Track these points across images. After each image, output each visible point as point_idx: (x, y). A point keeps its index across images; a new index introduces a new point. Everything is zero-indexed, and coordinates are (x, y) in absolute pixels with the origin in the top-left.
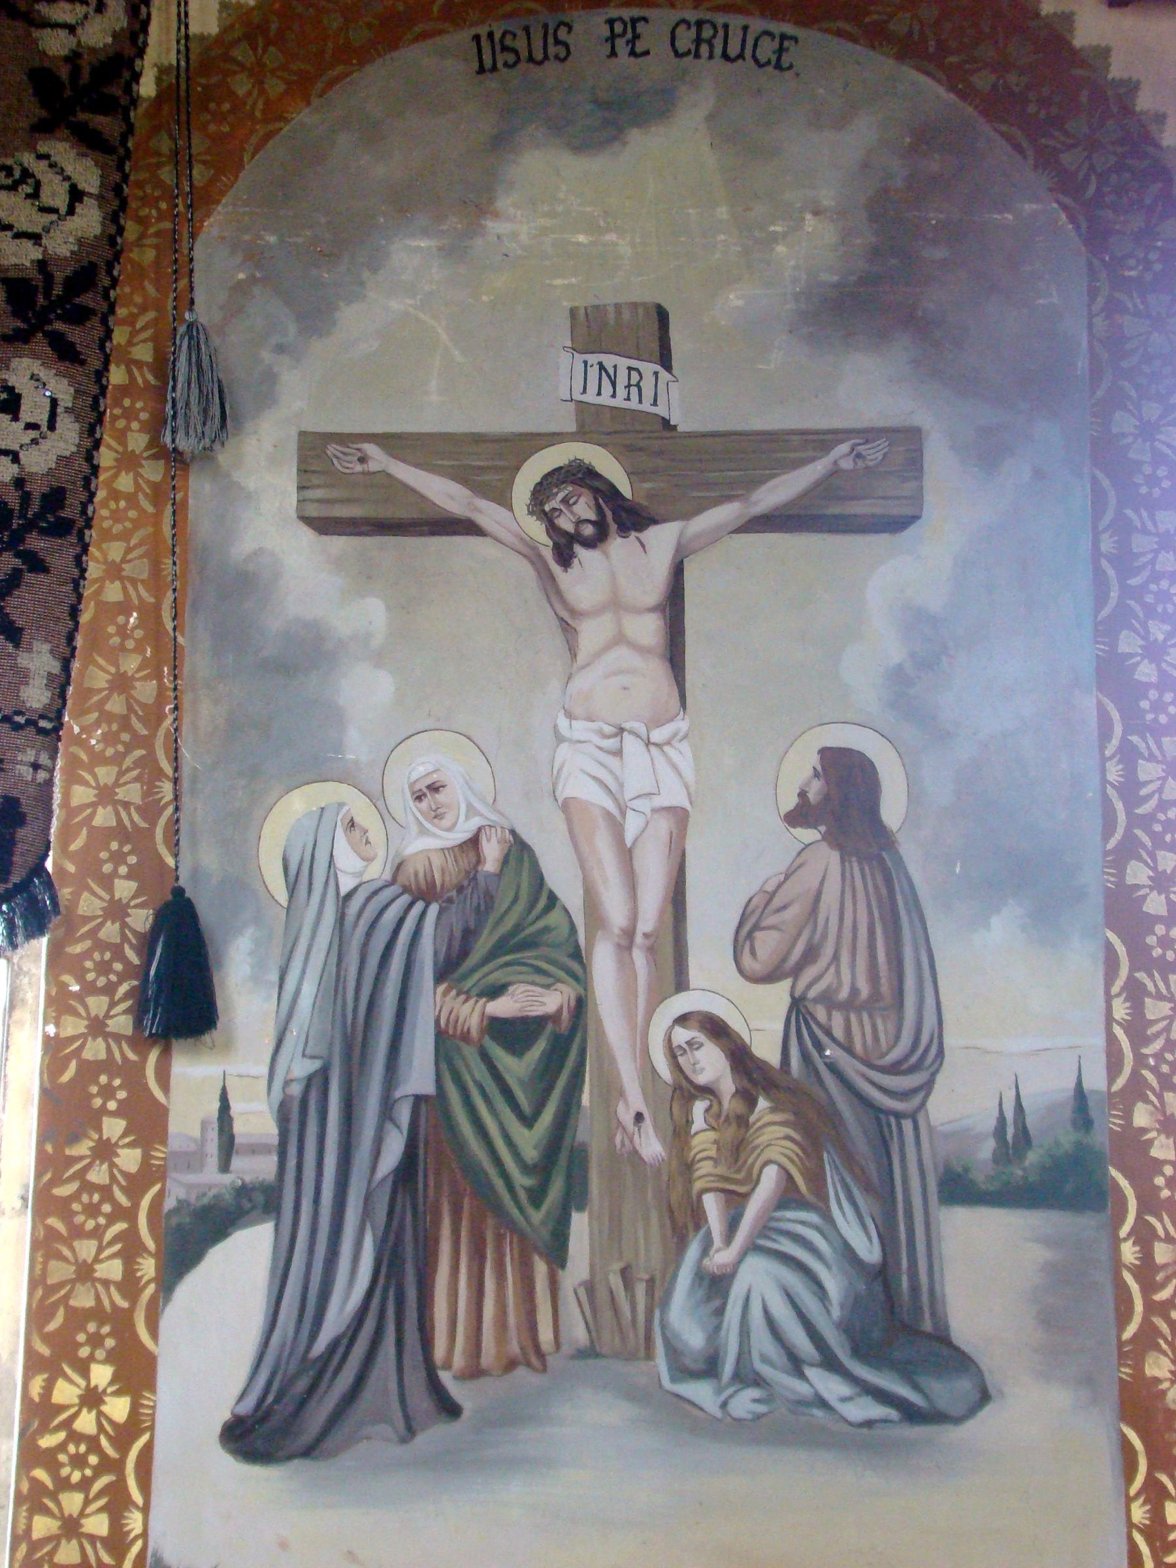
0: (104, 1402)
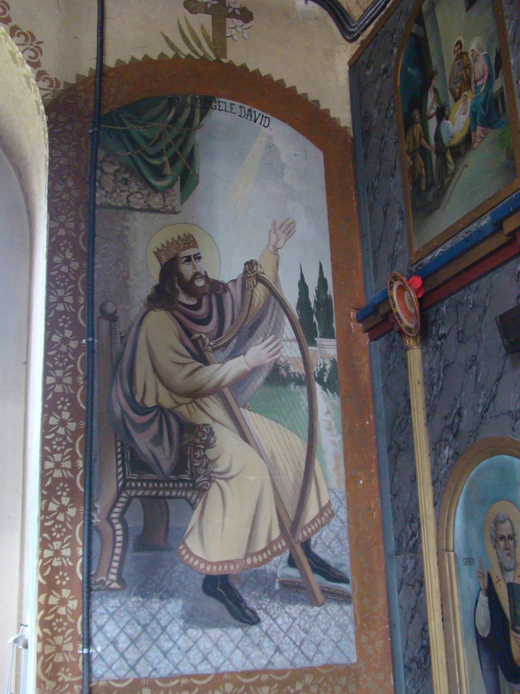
0: (69, 342)
